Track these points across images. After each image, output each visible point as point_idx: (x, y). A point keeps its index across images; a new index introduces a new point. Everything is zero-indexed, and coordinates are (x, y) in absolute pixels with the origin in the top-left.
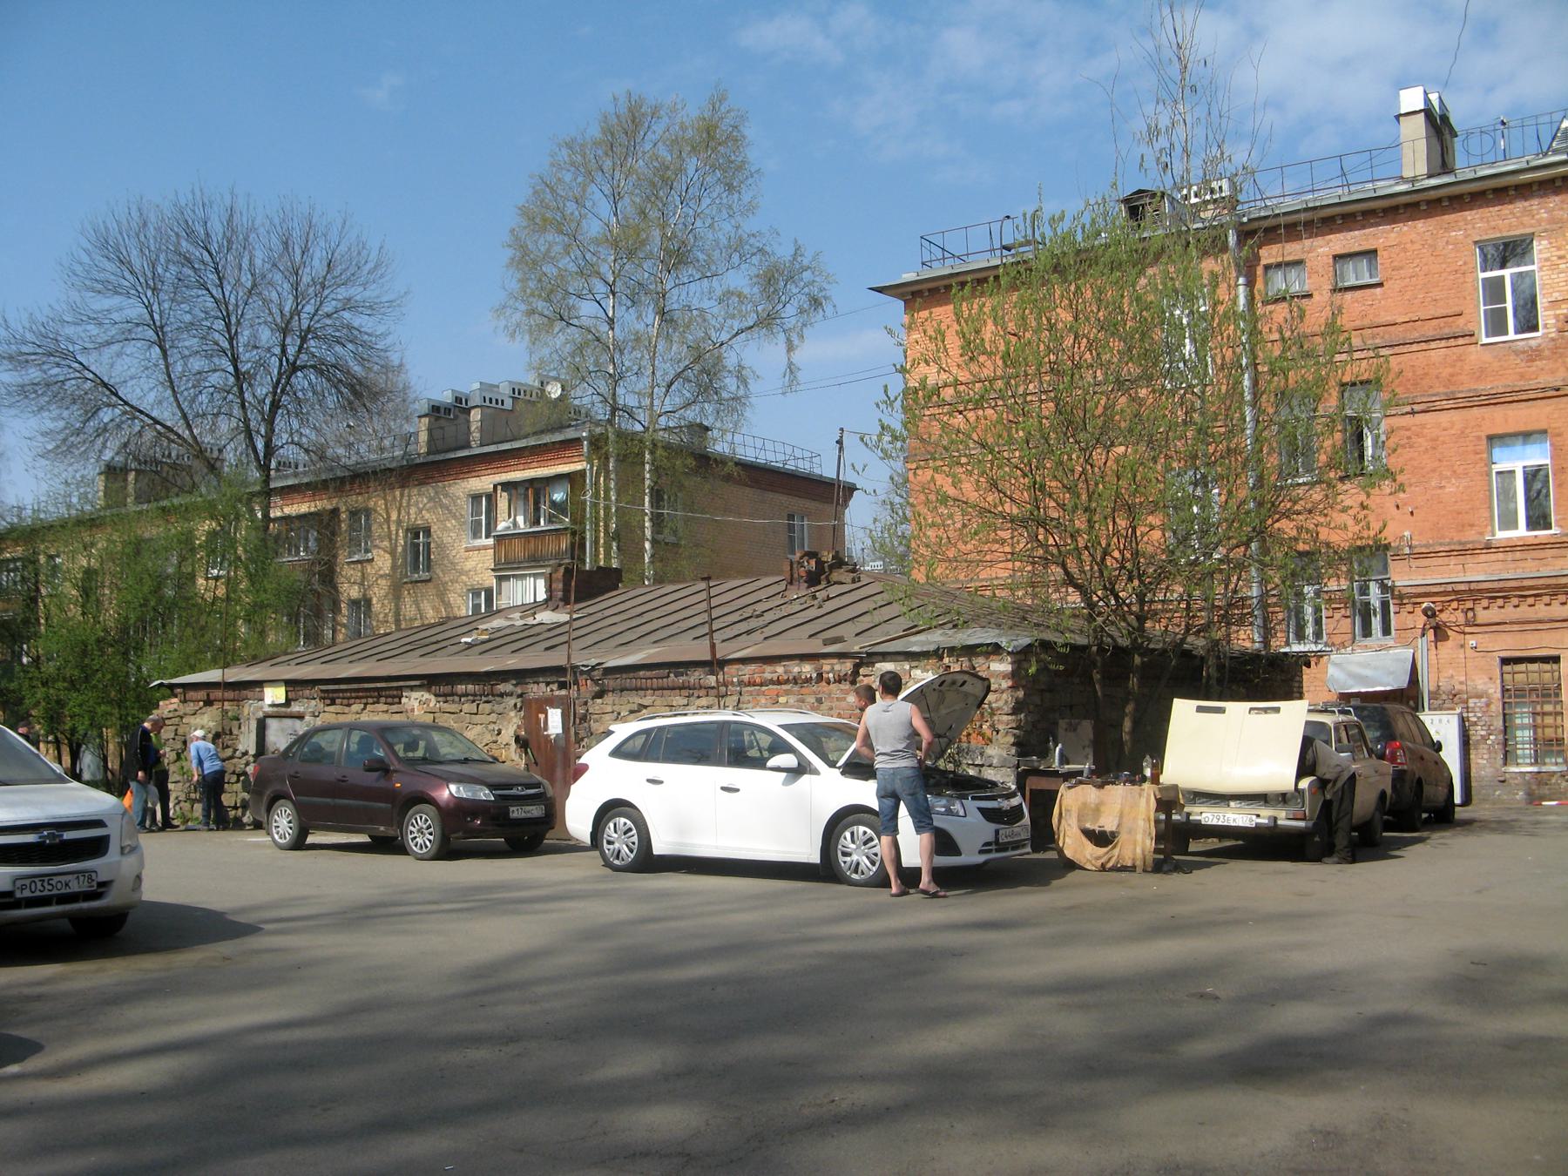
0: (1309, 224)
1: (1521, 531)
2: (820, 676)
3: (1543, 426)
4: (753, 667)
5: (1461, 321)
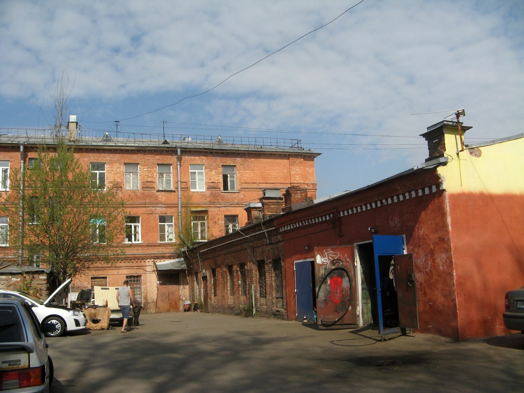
0: (155, 151)
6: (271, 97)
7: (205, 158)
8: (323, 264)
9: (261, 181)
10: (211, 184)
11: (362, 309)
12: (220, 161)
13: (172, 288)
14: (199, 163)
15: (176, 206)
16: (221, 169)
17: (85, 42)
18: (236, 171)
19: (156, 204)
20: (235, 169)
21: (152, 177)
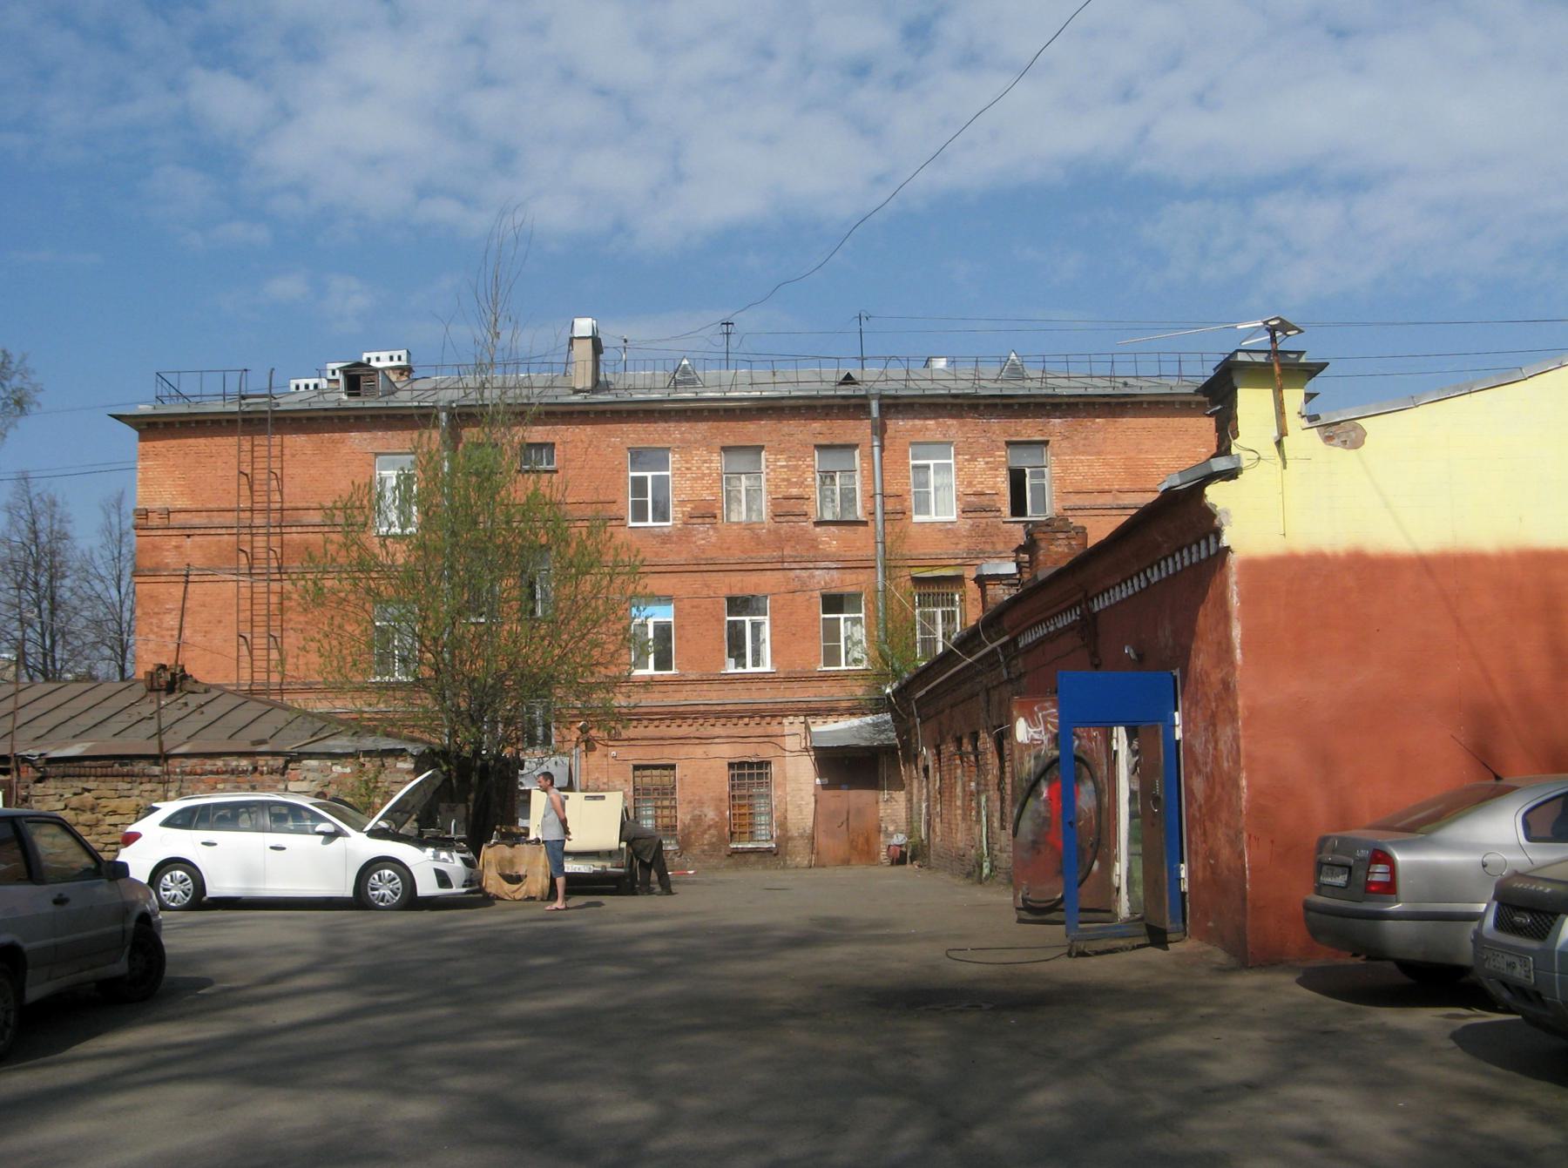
1: (650, 671)
2: (255, 769)
3: (670, 593)
4: (194, 761)
5: (614, 507)
6: (1354, 185)
7: (955, 422)
8: (1032, 744)
9: (1127, 486)
10: (973, 498)
11: (1129, 870)
12: (999, 429)
13: (858, 797)
14: (939, 437)
15: (866, 566)
16: (1002, 455)
17: (766, 53)
18: (1049, 458)
19: (813, 558)
20: (1048, 451)
21: (801, 484)
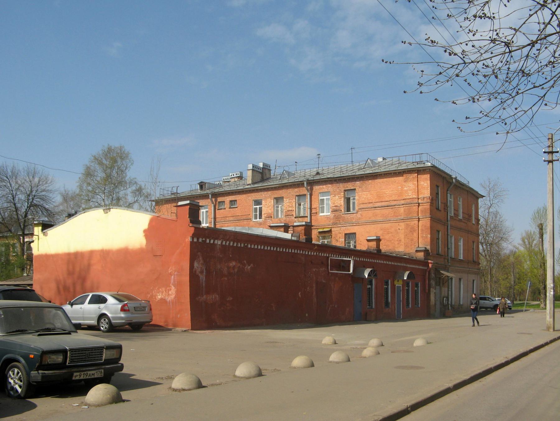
9: (377, 200)
12: (342, 186)
14: (326, 190)
